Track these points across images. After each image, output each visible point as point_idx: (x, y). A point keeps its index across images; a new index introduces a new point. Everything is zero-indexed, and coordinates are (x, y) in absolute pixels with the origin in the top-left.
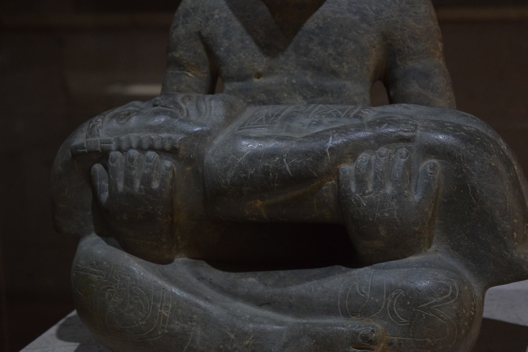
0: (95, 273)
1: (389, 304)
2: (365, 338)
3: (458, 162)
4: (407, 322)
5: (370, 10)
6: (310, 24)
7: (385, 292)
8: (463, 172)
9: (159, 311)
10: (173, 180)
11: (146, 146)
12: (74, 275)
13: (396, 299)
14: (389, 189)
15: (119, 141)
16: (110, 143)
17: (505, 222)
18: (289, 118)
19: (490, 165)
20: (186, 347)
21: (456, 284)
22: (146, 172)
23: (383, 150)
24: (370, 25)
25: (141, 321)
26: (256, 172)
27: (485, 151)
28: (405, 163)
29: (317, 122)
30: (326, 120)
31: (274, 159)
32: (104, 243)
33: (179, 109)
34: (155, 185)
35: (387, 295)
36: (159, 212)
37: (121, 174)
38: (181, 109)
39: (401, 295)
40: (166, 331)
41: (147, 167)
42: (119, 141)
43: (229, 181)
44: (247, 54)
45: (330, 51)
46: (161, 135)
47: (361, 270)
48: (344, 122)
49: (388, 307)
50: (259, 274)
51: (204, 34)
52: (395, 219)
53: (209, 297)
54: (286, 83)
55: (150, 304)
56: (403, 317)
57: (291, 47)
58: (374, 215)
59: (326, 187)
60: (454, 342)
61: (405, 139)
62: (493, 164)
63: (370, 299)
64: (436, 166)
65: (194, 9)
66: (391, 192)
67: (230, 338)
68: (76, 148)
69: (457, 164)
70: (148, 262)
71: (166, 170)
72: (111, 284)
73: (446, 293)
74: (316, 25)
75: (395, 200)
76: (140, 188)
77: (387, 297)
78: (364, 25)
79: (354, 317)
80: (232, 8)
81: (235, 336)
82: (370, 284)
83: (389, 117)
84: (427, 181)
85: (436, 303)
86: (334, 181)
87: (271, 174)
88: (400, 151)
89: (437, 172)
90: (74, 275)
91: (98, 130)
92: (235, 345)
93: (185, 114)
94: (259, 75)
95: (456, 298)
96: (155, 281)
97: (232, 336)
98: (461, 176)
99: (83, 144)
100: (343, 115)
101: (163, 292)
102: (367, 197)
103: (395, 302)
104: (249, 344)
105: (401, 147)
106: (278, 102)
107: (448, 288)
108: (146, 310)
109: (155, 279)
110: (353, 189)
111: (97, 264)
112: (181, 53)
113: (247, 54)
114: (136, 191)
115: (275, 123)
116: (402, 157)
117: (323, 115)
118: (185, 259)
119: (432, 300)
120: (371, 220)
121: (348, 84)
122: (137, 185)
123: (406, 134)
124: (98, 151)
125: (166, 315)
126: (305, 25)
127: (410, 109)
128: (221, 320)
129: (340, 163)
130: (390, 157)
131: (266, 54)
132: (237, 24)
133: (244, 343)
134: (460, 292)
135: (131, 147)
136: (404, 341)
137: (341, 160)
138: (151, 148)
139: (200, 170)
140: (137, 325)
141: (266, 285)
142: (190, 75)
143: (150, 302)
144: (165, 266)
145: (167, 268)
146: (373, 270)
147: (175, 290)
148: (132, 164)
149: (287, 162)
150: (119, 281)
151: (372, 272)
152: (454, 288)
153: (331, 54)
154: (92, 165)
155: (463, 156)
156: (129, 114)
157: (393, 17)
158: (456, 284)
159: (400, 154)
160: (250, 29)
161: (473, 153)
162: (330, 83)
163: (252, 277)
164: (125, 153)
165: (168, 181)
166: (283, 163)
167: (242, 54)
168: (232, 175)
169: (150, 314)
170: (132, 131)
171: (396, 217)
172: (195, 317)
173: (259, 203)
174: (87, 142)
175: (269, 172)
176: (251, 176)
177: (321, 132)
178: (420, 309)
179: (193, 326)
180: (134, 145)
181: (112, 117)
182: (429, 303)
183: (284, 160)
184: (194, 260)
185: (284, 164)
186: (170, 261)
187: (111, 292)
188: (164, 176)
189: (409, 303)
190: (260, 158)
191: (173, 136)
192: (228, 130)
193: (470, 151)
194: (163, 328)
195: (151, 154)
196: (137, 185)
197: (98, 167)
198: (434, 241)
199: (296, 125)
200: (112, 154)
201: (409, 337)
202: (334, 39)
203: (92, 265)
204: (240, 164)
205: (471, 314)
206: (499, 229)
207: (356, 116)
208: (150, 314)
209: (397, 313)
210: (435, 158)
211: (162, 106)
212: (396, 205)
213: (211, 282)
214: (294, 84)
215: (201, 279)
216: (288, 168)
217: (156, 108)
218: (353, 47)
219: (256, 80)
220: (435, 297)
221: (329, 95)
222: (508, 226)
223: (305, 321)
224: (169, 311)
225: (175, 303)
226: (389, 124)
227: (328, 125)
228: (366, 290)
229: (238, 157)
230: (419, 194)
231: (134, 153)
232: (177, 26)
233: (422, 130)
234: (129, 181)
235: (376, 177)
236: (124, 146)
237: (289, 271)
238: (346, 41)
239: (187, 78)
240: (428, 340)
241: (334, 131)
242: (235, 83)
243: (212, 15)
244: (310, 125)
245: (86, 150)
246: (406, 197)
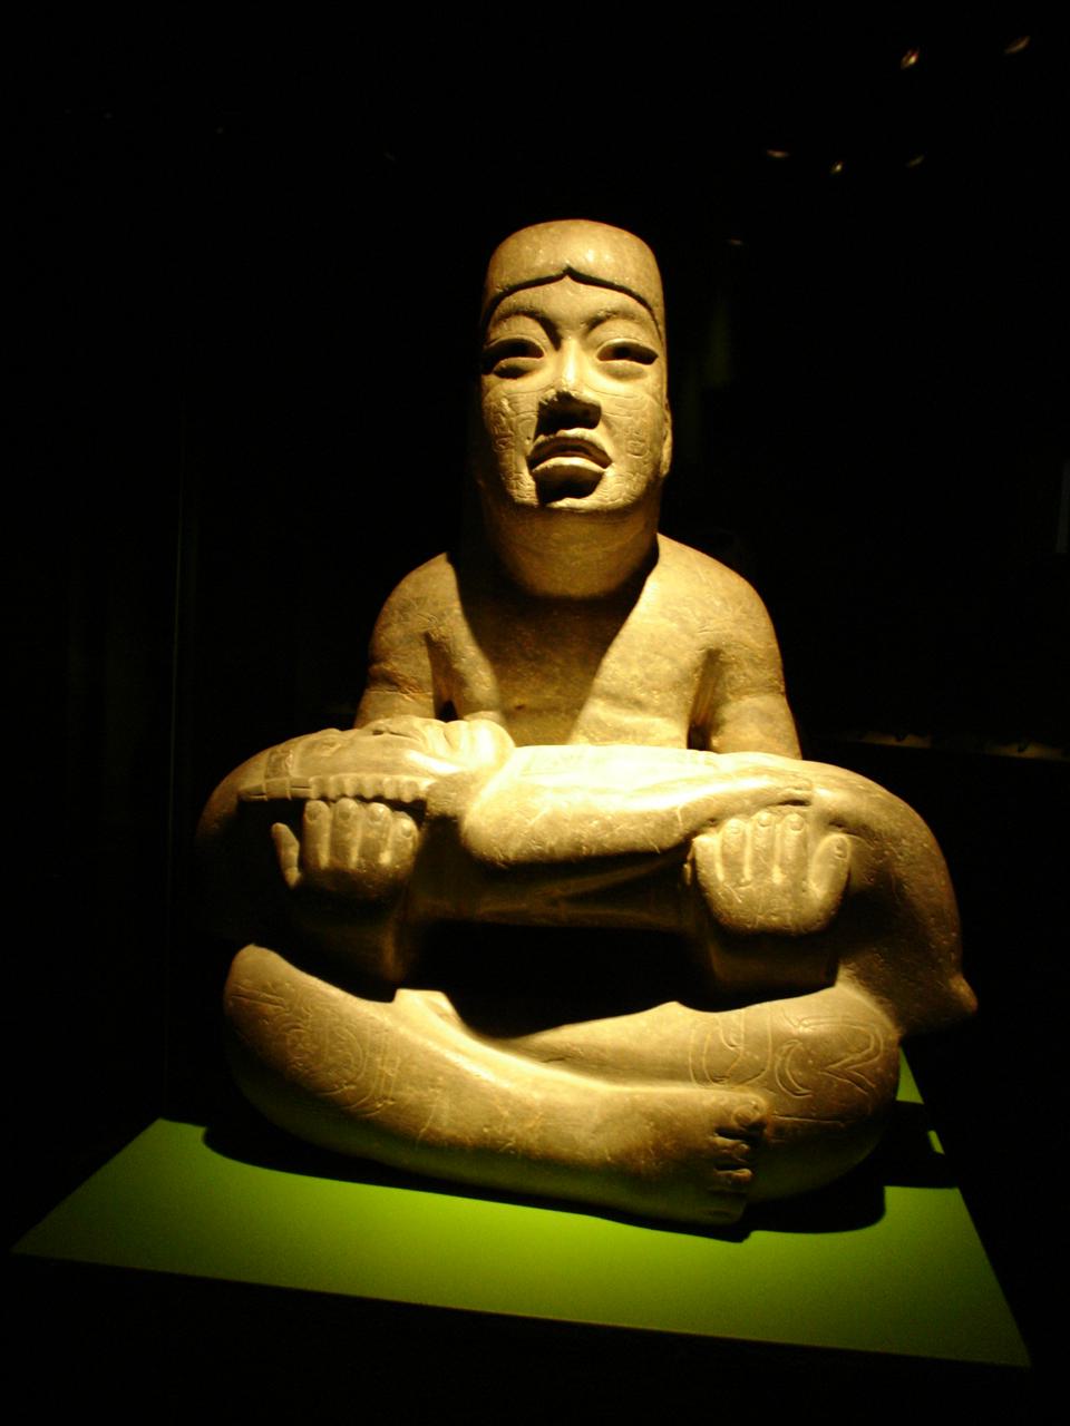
15: (322, 783)
25: (347, 1084)
31: (591, 822)
67: (502, 1116)
71: (404, 834)
72: (299, 1021)
82: (743, 1029)
99: (260, 787)
102: (743, 889)
103: (788, 1059)
105: (791, 813)
107: (869, 1037)
119: (846, 1057)
123: (799, 793)
125: (390, 1074)
138: (379, 799)
142: (407, 698)
152: (878, 1041)
153: (636, 676)
157: (725, 629)
164: (332, 804)
174: (267, 784)
182: (843, 1062)
197: (283, 829)
200: (310, 805)
204: (532, 828)
212: (790, 902)
224: (396, 1069)
228: (738, 1040)
229: (529, 818)
231: (351, 805)
232: (389, 625)
234: (339, 848)
236: (332, 793)
238: (658, 657)
239: (402, 702)
245: (265, 797)
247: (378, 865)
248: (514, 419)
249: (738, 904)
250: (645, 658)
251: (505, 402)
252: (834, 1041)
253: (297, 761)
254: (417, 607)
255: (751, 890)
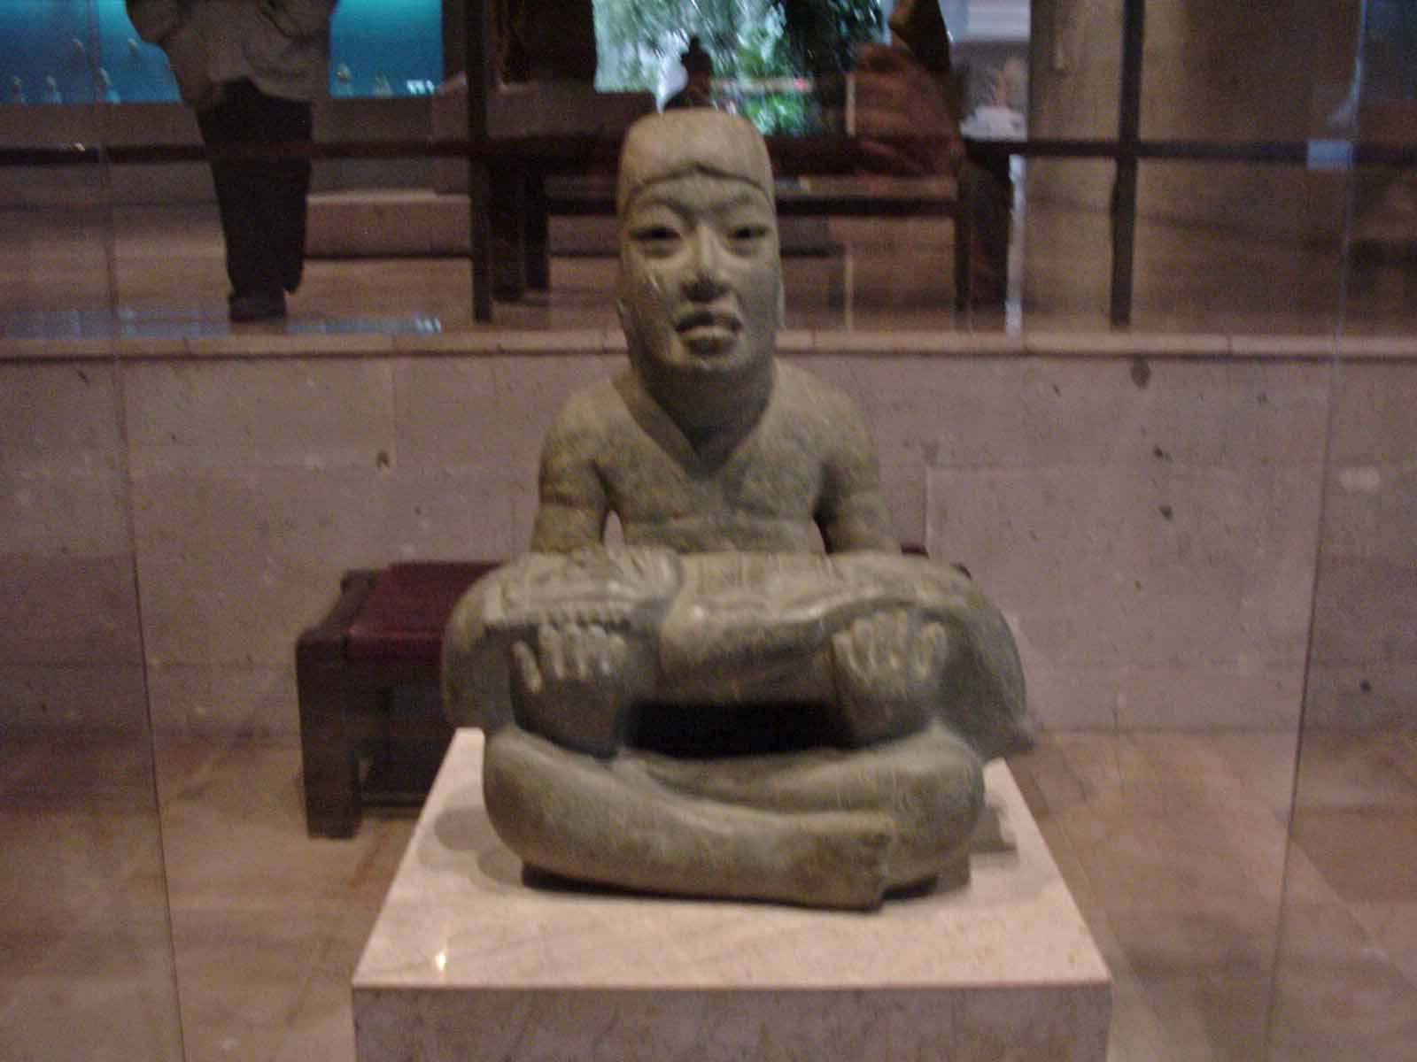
11: (587, 618)
14: (894, 662)
66: (568, 464)
94: (677, 516)
162: (765, 525)
231: (573, 629)
234: (570, 664)
236: (559, 618)
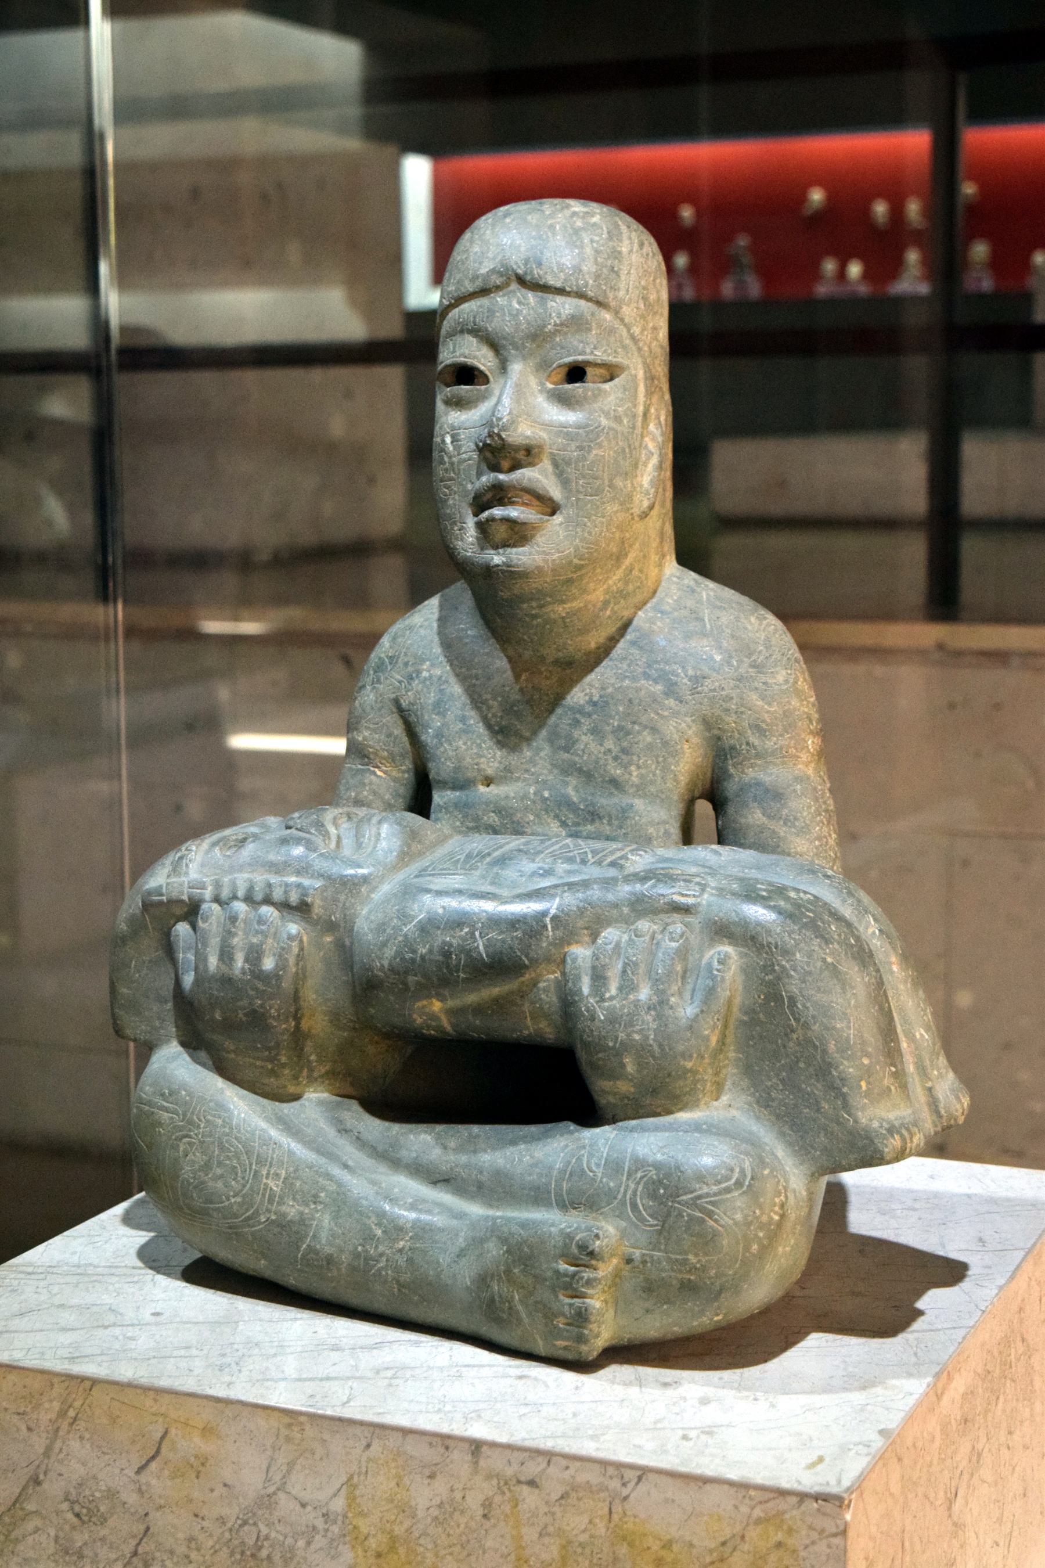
0: (166, 1110)
1: (630, 1192)
2: (583, 1247)
3: (767, 953)
4: (657, 1225)
5: (682, 675)
6: (577, 696)
7: (626, 1169)
8: (774, 971)
9: (265, 1181)
10: (300, 957)
12: (135, 1110)
13: (642, 1183)
14: (644, 993)
15: (218, 885)
16: (204, 888)
17: (845, 1062)
18: (502, 861)
19: (824, 960)
20: (304, 1246)
21: (747, 1165)
22: (255, 940)
23: (644, 925)
24: (681, 702)
25: (234, 1197)
26: (430, 951)
27: (816, 937)
28: (678, 951)
29: (545, 871)
30: (562, 867)
31: (461, 930)
32: (188, 1059)
33: (324, 836)
34: (268, 964)
35: (629, 1175)
36: (273, 1011)
37: (215, 942)
38: (326, 835)
39: (651, 1178)
40: (273, 1217)
41: (257, 932)
42: (218, 885)
43: (386, 963)
44: (469, 743)
45: (609, 743)
46: (285, 879)
47: (597, 1130)
48: (592, 872)
49: (628, 1197)
50: (439, 1128)
51: (404, 704)
52: (651, 1046)
53: (350, 1163)
54: (532, 797)
55: (251, 1169)
56: (651, 1216)
57: (544, 733)
58: (617, 1037)
59: (545, 984)
60: (737, 1265)
61: (681, 909)
62: (829, 960)
63: (601, 1182)
64: (730, 958)
65: (391, 658)
68: (149, 893)
69: (765, 955)
70: (256, 1097)
71: (288, 939)
72: (190, 1130)
73: (727, 1179)
74: (587, 698)
75: (653, 1013)
76: (243, 968)
77: (628, 1179)
78: (671, 702)
79: (574, 1211)
80: (451, 663)
81: (384, 1232)
82: (605, 1155)
83: (663, 869)
84: (711, 984)
85: (708, 1195)
86: (558, 975)
87: (454, 957)
88: (671, 928)
89: (730, 969)
90: (135, 1110)
91: (187, 865)
92: (381, 1248)
93: (333, 845)
94: (488, 781)
95: (745, 1188)
96: (262, 1130)
97: (379, 1232)
98: (771, 977)
99: (161, 887)
100: (593, 861)
101: (273, 1150)
102: (606, 1004)
103: (640, 1188)
104: (403, 1248)
105: (674, 923)
106: (518, 832)
107: (732, 1170)
108: (243, 1178)
109: (263, 1125)
110: (586, 990)
111: (170, 1095)
112: (366, 734)
113: (469, 743)
114: (237, 972)
115: (477, 868)
116: (672, 939)
117: (560, 858)
118: (325, 1095)
119: (700, 1188)
120: (611, 1044)
121: (639, 804)
122: (239, 962)
124: (182, 901)
125: (275, 1188)
126: (569, 697)
127: (721, 854)
128: (364, 1202)
129: (569, 944)
130: (653, 938)
131: (501, 744)
132: (456, 689)
133: (396, 1246)
134: (752, 1178)
135: (235, 897)
136: (652, 1257)
137: (569, 937)
138: (268, 901)
139: (347, 943)
140: (227, 1203)
141: (445, 1148)
142: (379, 773)
143: (251, 1164)
144: (285, 1105)
145: (286, 1108)
146: (615, 1132)
147: (296, 1147)
148: (234, 927)
149: (481, 937)
150: (202, 1126)
151: (612, 1136)
152: (742, 1171)
153: (610, 750)
154: (174, 925)
155: (776, 944)
156: (244, 840)
158: (747, 1165)
159: (671, 933)
160: (477, 701)
161: (794, 939)
162: (606, 802)
163: (426, 1132)
165: (292, 961)
166: (475, 938)
167: (461, 743)
168: (393, 953)
169: (248, 1186)
170: (241, 869)
171: (651, 1042)
172: (322, 1195)
173: (437, 1006)
174: (168, 884)
175: (451, 954)
176: (423, 958)
177: (545, 888)
178: (679, 1203)
179: (318, 1211)
180: (241, 894)
181: (214, 844)
182: (695, 1194)
183: (477, 933)
184: (339, 1099)
185: (475, 941)
186: (296, 1097)
187: (189, 1143)
188: (283, 949)
189: (662, 1191)
190: (438, 928)
191: (306, 882)
192: (400, 876)
193: (790, 935)
194: (268, 1211)
195: (266, 910)
196: (239, 962)
197: (182, 929)
198: (726, 1087)
199: (510, 873)
200: (205, 906)
201: (660, 1250)
202: (616, 724)
203: (163, 1095)
204: (406, 935)
205: (771, 1218)
206: (834, 1073)
207: (613, 864)
208: (248, 1186)
209: (641, 1208)
210: (730, 944)
211: (297, 829)
212: (654, 1020)
213: (358, 1138)
214: (547, 799)
215: (344, 1131)
216: (481, 948)
217: (289, 831)
218: (649, 739)
219: (482, 789)
220: (707, 1185)
221: (605, 821)
222: (851, 1070)
223: (499, 1214)
224: (280, 1183)
225: (291, 1169)
226: (659, 880)
227: (561, 877)
230: (695, 1004)
233: (712, 894)
234: (226, 955)
235: (624, 972)
236: (225, 894)
237: (488, 1127)
238: (637, 727)
240: (690, 1257)
241: (566, 888)
242: (449, 793)
243: (419, 672)
244: (534, 874)
245: (164, 898)
246: (671, 1008)
247: (261, 971)
248: (455, 459)
249: (600, 1020)
250: (620, 728)
251: (448, 439)
252: (813, 1169)
253: (199, 858)
254: (389, 668)
255: (615, 1006)
